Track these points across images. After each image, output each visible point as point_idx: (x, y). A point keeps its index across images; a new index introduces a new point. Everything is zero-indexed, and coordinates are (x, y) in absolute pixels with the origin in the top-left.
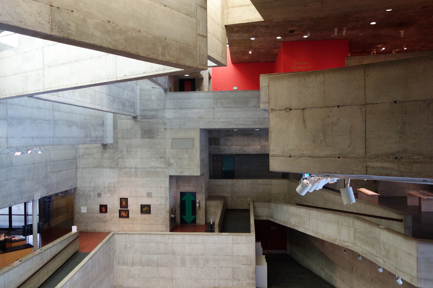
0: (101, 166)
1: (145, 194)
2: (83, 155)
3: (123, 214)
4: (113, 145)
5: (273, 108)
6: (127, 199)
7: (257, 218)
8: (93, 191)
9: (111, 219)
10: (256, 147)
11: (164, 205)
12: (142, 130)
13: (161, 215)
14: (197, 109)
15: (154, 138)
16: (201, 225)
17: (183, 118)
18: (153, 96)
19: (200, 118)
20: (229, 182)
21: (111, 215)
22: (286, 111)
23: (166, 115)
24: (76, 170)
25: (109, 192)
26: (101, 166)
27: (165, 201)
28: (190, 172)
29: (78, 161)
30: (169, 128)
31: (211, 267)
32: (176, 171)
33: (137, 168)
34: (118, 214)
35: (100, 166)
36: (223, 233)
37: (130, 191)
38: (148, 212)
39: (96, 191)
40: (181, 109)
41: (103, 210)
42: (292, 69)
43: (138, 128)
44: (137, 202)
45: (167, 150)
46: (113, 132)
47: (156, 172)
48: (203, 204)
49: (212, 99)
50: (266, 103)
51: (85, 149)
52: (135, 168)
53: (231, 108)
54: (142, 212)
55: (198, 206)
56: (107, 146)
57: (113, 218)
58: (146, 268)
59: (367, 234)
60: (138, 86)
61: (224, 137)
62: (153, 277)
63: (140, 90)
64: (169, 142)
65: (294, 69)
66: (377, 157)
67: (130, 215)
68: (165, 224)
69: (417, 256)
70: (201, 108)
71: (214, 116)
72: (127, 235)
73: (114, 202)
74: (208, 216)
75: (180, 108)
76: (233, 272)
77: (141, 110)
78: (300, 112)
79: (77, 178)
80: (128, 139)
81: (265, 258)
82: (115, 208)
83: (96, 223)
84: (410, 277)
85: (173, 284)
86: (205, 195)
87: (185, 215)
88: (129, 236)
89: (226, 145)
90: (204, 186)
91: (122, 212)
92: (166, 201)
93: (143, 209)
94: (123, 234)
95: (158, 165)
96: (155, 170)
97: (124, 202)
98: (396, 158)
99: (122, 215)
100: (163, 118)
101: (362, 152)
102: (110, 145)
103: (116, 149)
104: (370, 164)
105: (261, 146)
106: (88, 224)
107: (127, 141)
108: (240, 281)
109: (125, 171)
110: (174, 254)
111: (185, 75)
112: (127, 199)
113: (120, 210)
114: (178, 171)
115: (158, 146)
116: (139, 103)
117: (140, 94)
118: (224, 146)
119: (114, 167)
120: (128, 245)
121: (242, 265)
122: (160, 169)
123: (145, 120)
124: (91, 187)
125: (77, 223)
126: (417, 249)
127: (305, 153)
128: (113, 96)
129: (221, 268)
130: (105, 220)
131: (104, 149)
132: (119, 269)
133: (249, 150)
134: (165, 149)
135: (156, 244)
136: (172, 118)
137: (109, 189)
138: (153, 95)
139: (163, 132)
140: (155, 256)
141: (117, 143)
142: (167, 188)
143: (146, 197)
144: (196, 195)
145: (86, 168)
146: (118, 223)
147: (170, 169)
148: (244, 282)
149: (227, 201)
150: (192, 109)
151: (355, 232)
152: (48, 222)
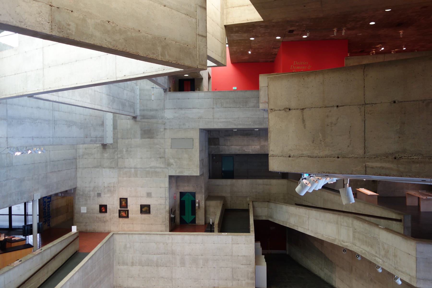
0: (100, 166)
1: (145, 194)
2: (83, 155)
3: (123, 214)
4: (112, 145)
5: (272, 108)
6: (126, 199)
7: (257, 218)
8: (93, 191)
9: (110, 219)
10: (255, 147)
11: (164, 205)
12: (141, 130)
13: (161, 215)
14: (196, 109)
15: (154, 138)
16: (200, 225)
17: (183, 118)
18: (153, 96)
19: (200, 118)
20: (229, 182)
21: (110, 215)
22: (286, 111)
23: (166, 115)
24: (76, 170)
25: (109, 192)
26: (100, 166)
27: (165, 201)
28: (190, 172)
29: (78, 161)
30: (168, 128)
31: (211, 267)
32: (176, 171)
33: (137, 168)
34: (118, 214)
35: (100, 166)
36: (223, 233)
37: (130, 191)
38: (148, 212)
39: (96, 191)
40: (181, 109)
41: (103, 210)
42: (291, 69)
43: (137, 128)
44: (137, 202)
45: (167, 150)
46: (112, 132)
47: (156, 172)
48: (202, 204)
49: (211, 99)
50: (266, 103)
51: (85, 149)
52: (135, 168)
53: (231, 108)
54: (142, 212)
55: (198, 206)
56: (107, 146)
57: (112, 218)
58: (146, 268)
59: (366, 234)
60: (138, 86)
61: (223, 137)
62: (153, 277)
63: (139, 90)
64: (168, 142)
65: (294, 69)
66: (376, 157)
67: (130, 215)
68: (164, 224)
69: (416, 256)
70: (201, 108)
71: (213, 116)
72: (127, 235)
73: (114, 202)
74: (208, 216)
75: (179, 108)
76: (232, 272)
77: (140, 110)
78: (299, 112)
79: (77, 178)
80: (127, 139)
81: (265, 258)
82: (115, 208)
83: (95, 223)
84: (410, 277)
85: (172, 284)
86: (204, 195)
87: (184, 215)
88: (129, 236)
89: (226, 145)
90: (203, 186)
91: (122, 212)
92: (166, 201)
93: (143, 209)
94: (122, 234)
95: (158, 165)
96: (155, 170)
97: (123, 202)
98: (395, 158)
99: (122, 215)
100: (162, 118)
101: (361, 152)
102: (110, 145)
103: (116, 149)
104: (370, 164)
105: (260, 146)
106: (87, 224)
107: (127, 141)
108: (240, 281)
109: (124, 171)
110: (174, 254)
111: (185, 75)
112: (126, 199)
113: (119, 210)
114: (178, 171)
115: (157, 146)
116: (139, 103)
117: (140, 94)
118: (224, 146)
119: (114, 167)
120: (128, 245)
121: (242, 265)
122: (159, 169)
123: (144, 120)
124: (91, 187)
125: (77, 223)
126: (416, 249)
127: (305, 153)
128: (113, 96)
129: (221, 268)
130: (105, 220)
131: (104, 149)
132: (118, 269)
133: (249, 150)
134: (165, 149)
135: (156, 244)
136: (172, 118)
137: (109, 189)
138: (153, 95)
139: (162, 132)
140: (155, 256)
141: (117, 143)
142: (166, 188)
143: (145, 197)
144: (196, 195)
145: (86, 168)
146: (118, 223)
147: (169, 169)
148: (244, 282)
149: (226, 201)
150: (191, 109)
151: (354, 232)
152: (48, 222)
